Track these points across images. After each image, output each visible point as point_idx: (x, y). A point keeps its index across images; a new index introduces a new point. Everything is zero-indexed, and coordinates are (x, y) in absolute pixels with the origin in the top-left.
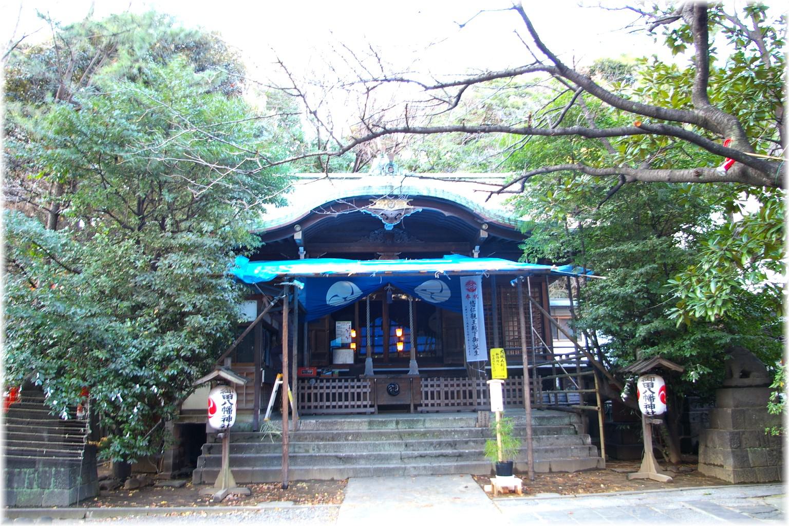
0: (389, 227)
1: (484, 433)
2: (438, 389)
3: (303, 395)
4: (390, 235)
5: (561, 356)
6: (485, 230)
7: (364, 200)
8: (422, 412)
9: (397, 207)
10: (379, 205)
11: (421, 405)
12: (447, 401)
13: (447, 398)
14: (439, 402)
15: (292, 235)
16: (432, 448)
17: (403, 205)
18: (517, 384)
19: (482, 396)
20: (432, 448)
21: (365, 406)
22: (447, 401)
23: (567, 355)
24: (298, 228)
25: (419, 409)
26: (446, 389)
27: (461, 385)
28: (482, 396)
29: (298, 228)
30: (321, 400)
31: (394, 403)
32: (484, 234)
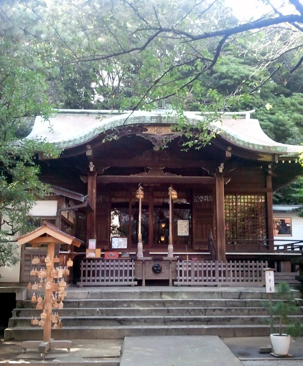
0: (156, 149)
1: (227, 303)
2: (214, 269)
3: (260, 276)
4: (154, 152)
5: (278, 246)
6: (229, 151)
7: (142, 127)
8: (177, 286)
9: (164, 133)
10: (151, 131)
11: (176, 280)
12: (196, 278)
13: (196, 276)
14: (190, 278)
15: (84, 152)
16: (188, 314)
17: (168, 131)
18: (253, 267)
19: (222, 275)
20: (188, 314)
21: (130, 280)
22: (196, 278)
23: (285, 246)
24: (89, 147)
25: (175, 283)
26: (220, 269)
27: (231, 266)
28: (222, 275)
29: (89, 147)
30: (98, 276)
31: (157, 278)
32: (228, 154)
